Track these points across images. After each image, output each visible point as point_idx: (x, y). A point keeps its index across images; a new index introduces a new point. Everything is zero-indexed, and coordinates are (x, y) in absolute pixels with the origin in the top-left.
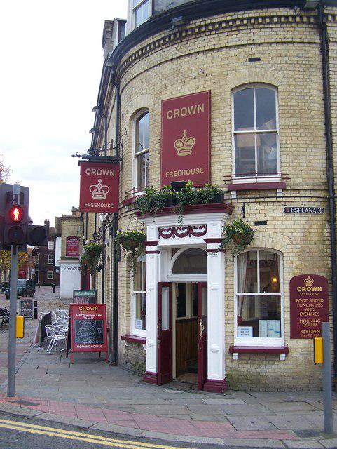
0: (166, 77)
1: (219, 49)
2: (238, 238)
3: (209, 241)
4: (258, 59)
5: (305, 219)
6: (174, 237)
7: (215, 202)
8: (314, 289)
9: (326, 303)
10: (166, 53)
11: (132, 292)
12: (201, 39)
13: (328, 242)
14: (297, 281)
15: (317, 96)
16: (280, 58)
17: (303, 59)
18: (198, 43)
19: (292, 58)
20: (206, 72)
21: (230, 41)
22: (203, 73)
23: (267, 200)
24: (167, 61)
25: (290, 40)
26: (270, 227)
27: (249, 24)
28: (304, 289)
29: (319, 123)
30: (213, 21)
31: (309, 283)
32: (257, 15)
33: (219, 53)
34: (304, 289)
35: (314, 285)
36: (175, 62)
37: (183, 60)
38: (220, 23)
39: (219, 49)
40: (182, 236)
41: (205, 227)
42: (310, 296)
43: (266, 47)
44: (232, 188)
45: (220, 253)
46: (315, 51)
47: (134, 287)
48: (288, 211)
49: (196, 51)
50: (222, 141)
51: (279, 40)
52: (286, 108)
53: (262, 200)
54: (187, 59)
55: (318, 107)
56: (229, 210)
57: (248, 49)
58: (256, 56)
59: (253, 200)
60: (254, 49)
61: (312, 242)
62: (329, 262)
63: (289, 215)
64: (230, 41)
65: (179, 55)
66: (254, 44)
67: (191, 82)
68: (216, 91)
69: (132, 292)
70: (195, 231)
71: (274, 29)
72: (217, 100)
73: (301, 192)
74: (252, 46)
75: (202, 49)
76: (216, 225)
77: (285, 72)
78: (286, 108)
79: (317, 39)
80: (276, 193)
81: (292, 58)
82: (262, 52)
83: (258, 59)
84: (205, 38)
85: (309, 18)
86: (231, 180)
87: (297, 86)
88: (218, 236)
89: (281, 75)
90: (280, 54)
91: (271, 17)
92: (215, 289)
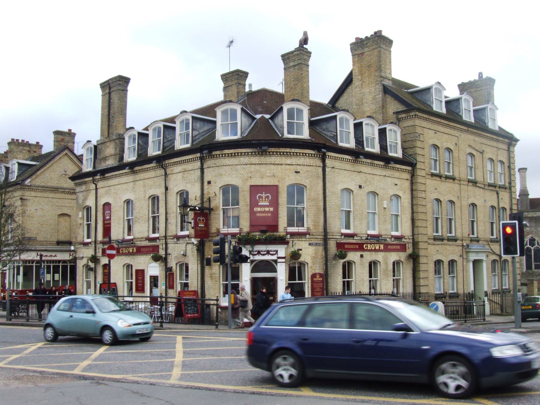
0: (251, 172)
1: (281, 164)
2: (295, 255)
3: (279, 258)
4: (299, 172)
5: (315, 248)
6: (259, 255)
7: (282, 241)
8: (320, 279)
9: (323, 285)
10: (252, 159)
11: (85, 279)
12: (272, 157)
13: (324, 259)
14: (314, 276)
15: (321, 192)
16: (308, 173)
17: (316, 174)
18: (271, 159)
19: (312, 173)
20: (275, 175)
21: (287, 161)
22: (274, 176)
23: (302, 239)
24: (251, 164)
25: (312, 165)
26: (303, 251)
27: (296, 155)
28: (316, 279)
29: (321, 204)
30: (280, 151)
31: (318, 277)
32: (300, 152)
33: (281, 166)
34: (316, 279)
35: (320, 277)
36: (257, 166)
37: (261, 166)
38: (283, 152)
39: (281, 164)
40: (264, 255)
41: (277, 251)
42: (318, 282)
43: (302, 167)
44: (288, 233)
45: (284, 263)
46: (320, 170)
47: (86, 278)
48: (310, 244)
49: (270, 163)
50: (283, 211)
51: (308, 164)
52: (310, 197)
53: (300, 239)
54: (264, 166)
55: (321, 197)
56: (287, 243)
57: (294, 166)
58: (298, 171)
59: (297, 239)
60: (297, 167)
61: (319, 258)
62: (324, 267)
63: (310, 246)
64: (287, 161)
65: (260, 163)
66: (297, 165)
67: (266, 178)
68: (280, 185)
69: (85, 279)
70: (271, 253)
71: (306, 159)
72: (280, 190)
73: (315, 236)
74: (296, 166)
75: (273, 163)
76: (282, 250)
77: (310, 180)
78: (310, 197)
79: (321, 165)
80: (306, 236)
81: (312, 173)
82: (301, 169)
83: (299, 172)
84: (275, 157)
85: (319, 155)
86: (287, 229)
87: (314, 187)
88: (284, 256)
89: (308, 181)
90: (308, 171)
91: (306, 154)
92: (282, 280)
